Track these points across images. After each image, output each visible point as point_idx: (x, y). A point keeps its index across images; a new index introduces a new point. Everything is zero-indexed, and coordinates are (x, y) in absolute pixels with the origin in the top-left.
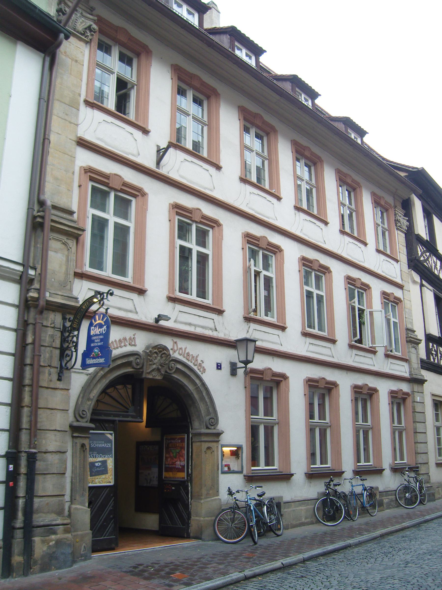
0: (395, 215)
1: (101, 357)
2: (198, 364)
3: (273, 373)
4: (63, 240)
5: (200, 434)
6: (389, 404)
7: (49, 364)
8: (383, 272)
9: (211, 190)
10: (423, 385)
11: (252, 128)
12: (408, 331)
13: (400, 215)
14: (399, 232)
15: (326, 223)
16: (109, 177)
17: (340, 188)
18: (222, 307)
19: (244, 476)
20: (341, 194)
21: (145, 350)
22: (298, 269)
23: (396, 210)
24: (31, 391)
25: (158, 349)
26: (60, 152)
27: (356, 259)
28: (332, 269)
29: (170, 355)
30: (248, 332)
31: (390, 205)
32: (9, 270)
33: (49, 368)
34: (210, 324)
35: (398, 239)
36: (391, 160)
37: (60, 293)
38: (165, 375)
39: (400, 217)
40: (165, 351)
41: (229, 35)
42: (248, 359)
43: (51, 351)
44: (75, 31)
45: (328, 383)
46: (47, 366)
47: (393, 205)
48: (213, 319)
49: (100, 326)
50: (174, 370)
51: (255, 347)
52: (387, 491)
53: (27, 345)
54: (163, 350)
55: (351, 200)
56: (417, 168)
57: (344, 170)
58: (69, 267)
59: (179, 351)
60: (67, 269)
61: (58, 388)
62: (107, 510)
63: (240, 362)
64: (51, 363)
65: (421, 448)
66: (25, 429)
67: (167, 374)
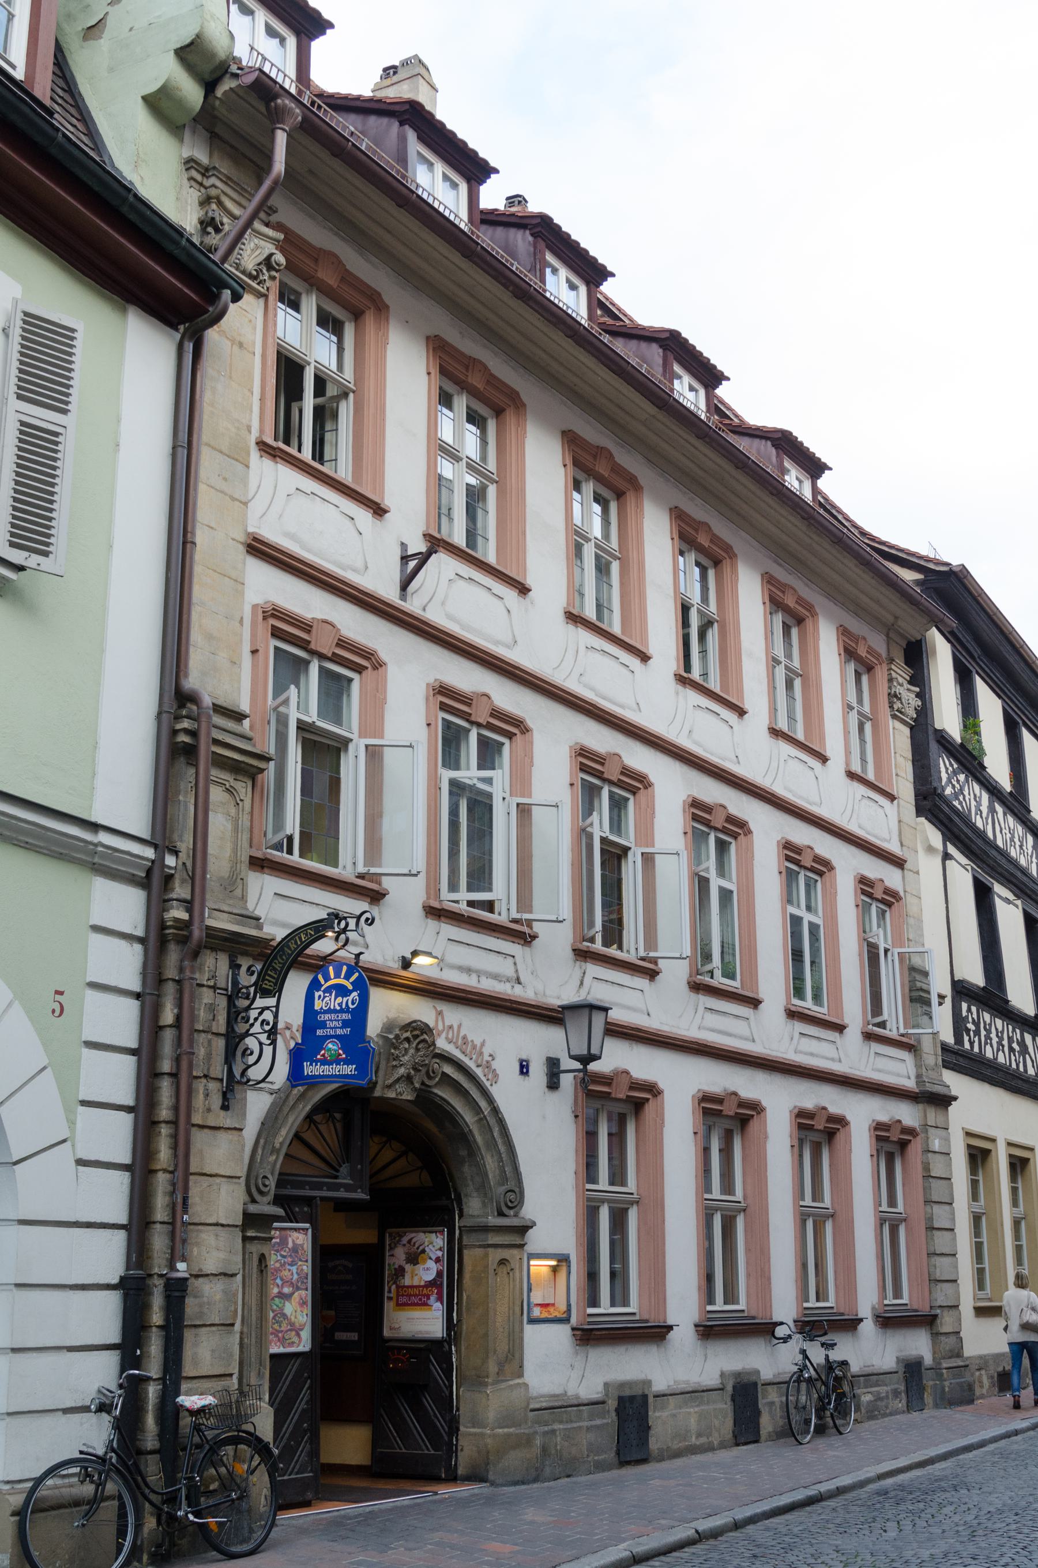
0: (891, 680)
1: (347, 1062)
2: (484, 1063)
3: (632, 1083)
4: (226, 783)
5: (486, 1229)
6: (872, 1156)
7: (206, 1073)
8: (860, 827)
9: (508, 647)
12: (913, 974)
13: (901, 680)
14: (898, 725)
15: (741, 712)
16: (311, 627)
17: (681, 559)
19: (573, 1329)
20: (682, 574)
21: (381, 1032)
22: (568, 781)
23: (891, 669)
24: (175, 1137)
25: (411, 1031)
27: (800, 797)
28: (752, 826)
29: (434, 1044)
30: (582, 983)
31: (878, 656)
32: (129, 857)
33: (204, 1081)
34: (505, 967)
35: (894, 741)
36: (884, 538)
37: (226, 908)
38: (420, 1089)
39: (901, 685)
40: (425, 1036)
41: (532, 235)
43: (209, 1041)
44: (237, 269)
45: (744, 1104)
46: (200, 1077)
47: (884, 655)
48: (513, 957)
49: (342, 991)
50: (437, 1079)
51: (607, 1023)
53: (161, 1028)
54: (422, 1034)
55: (708, 589)
56: (948, 564)
57: (781, 574)
58: (239, 845)
59: (448, 1034)
60: (235, 851)
61: (222, 1127)
63: (572, 1057)
64: (208, 1069)
66: (161, 1223)
67: (423, 1087)
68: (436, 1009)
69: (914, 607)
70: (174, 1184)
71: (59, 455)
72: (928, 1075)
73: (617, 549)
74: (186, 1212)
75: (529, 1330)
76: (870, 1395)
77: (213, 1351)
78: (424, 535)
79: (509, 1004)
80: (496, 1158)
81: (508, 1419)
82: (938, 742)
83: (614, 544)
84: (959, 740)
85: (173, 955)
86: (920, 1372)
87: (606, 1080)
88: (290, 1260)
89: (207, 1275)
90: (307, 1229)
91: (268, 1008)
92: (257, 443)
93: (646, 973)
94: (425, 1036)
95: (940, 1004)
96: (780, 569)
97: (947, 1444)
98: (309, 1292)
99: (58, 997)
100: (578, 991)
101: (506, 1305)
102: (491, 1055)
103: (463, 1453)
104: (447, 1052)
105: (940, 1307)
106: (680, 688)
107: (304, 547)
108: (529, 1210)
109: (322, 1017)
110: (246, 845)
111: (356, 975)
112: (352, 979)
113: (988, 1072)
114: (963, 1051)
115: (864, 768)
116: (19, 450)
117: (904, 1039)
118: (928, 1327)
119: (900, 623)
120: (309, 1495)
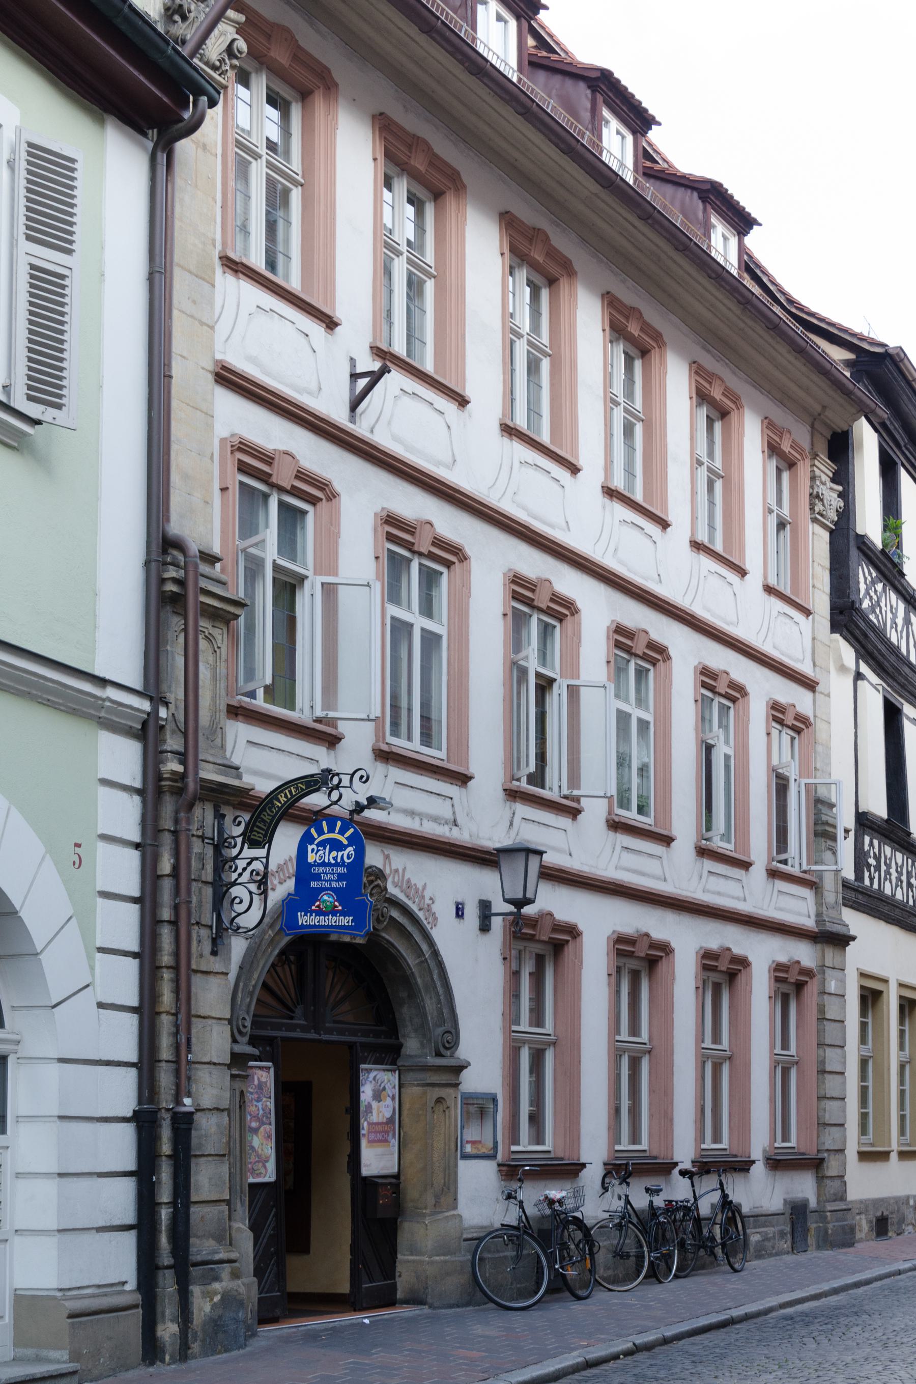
0: (813, 478)
1: (344, 914)
2: (426, 906)
3: (555, 925)
8: (774, 647)
9: (447, 467)
10: (845, 950)
11: (398, 177)
13: (824, 478)
14: (818, 529)
16: (273, 459)
18: (468, 769)
19: (499, 1165)
23: (814, 465)
24: (177, 981)
26: (188, 404)
28: (672, 652)
29: (386, 889)
30: (511, 824)
32: (129, 711)
33: (196, 927)
34: (442, 809)
36: (814, 309)
37: (211, 759)
39: (824, 484)
40: (379, 882)
42: (528, 896)
48: (451, 798)
50: (385, 923)
51: (541, 866)
52: (757, 1216)
53: (159, 877)
54: (376, 880)
55: (424, 231)
56: (883, 345)
57: (709, 362)
59: (394, 877)
61: (212, 972)
62: (264, 1236)
63: (507, 901)
65: (831, 1110)
68: (384, 854)
69: (845, 396)
70: (177, 1026)
71: (66, 300)
72: (828, 914)
73: (548, 345)
74: (189, 1051)
75: (462, 1164)
76: (758, 1236)
77: (210, 1179)
78: (371, 347)
79: (448, 847)
80: (434, 1000)
81: (443, 1248)
82: (859, 548)
83: (545, 339)
84: (880, 546)
85: (168, 806)
86: (805, 1212)
87: (533, 922)
88: (256, 1096)
89: (203, 1110)
90: (270, 1068)
91: (257, 859)
92: (220, 258)
93: (569, 813)
94: (379, 882)
95: (845, 838)
96: (708, 356)
97: (840, 1280)
98: (273, 1127)
99: (77, 850)
100: (508, 832)
101: (443, 1142)
102: (431, 899)
103: (401, 1279)
104: (394, 896)
105: (827, 1150)
106: (607, 501)
107: (268, 374)
108: (464, 1051)
109: (317, 870)
110: (223, 693)
111: (352, 830)
112: (347, 834)
113: (885, 909)
114: (863, 888)
115: (712, 538)
116: (30, 296)
117: (807, 876)
118: (814, 1171)
119: (828, 413)
120: (278, 1312)
